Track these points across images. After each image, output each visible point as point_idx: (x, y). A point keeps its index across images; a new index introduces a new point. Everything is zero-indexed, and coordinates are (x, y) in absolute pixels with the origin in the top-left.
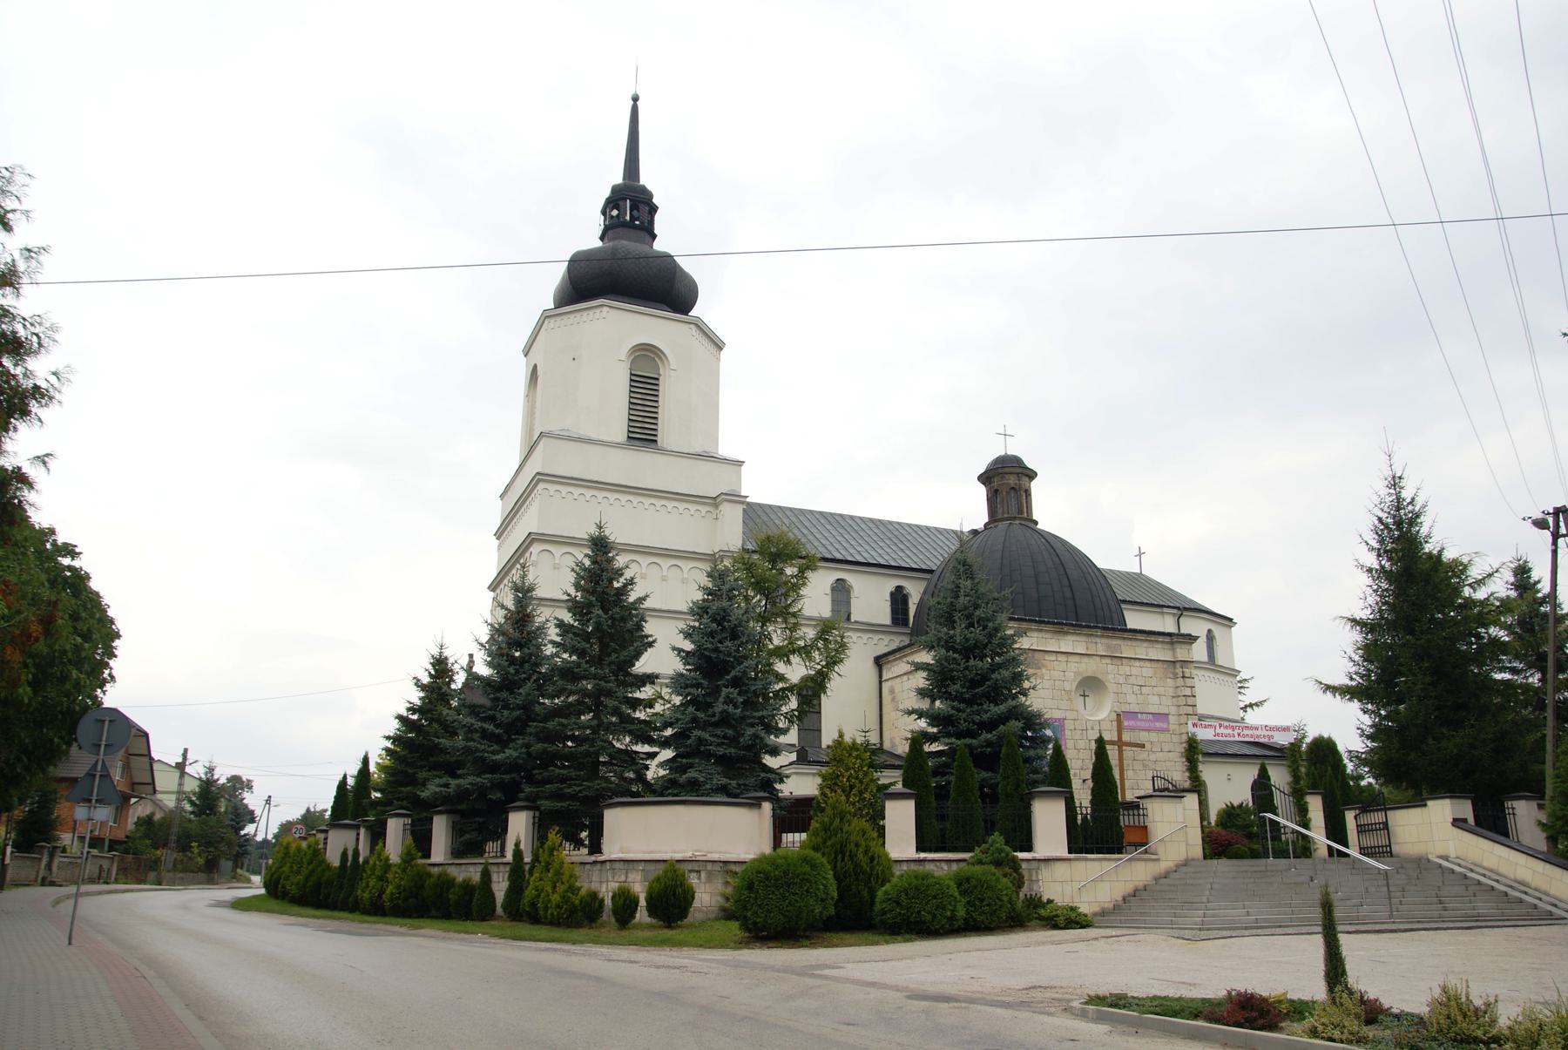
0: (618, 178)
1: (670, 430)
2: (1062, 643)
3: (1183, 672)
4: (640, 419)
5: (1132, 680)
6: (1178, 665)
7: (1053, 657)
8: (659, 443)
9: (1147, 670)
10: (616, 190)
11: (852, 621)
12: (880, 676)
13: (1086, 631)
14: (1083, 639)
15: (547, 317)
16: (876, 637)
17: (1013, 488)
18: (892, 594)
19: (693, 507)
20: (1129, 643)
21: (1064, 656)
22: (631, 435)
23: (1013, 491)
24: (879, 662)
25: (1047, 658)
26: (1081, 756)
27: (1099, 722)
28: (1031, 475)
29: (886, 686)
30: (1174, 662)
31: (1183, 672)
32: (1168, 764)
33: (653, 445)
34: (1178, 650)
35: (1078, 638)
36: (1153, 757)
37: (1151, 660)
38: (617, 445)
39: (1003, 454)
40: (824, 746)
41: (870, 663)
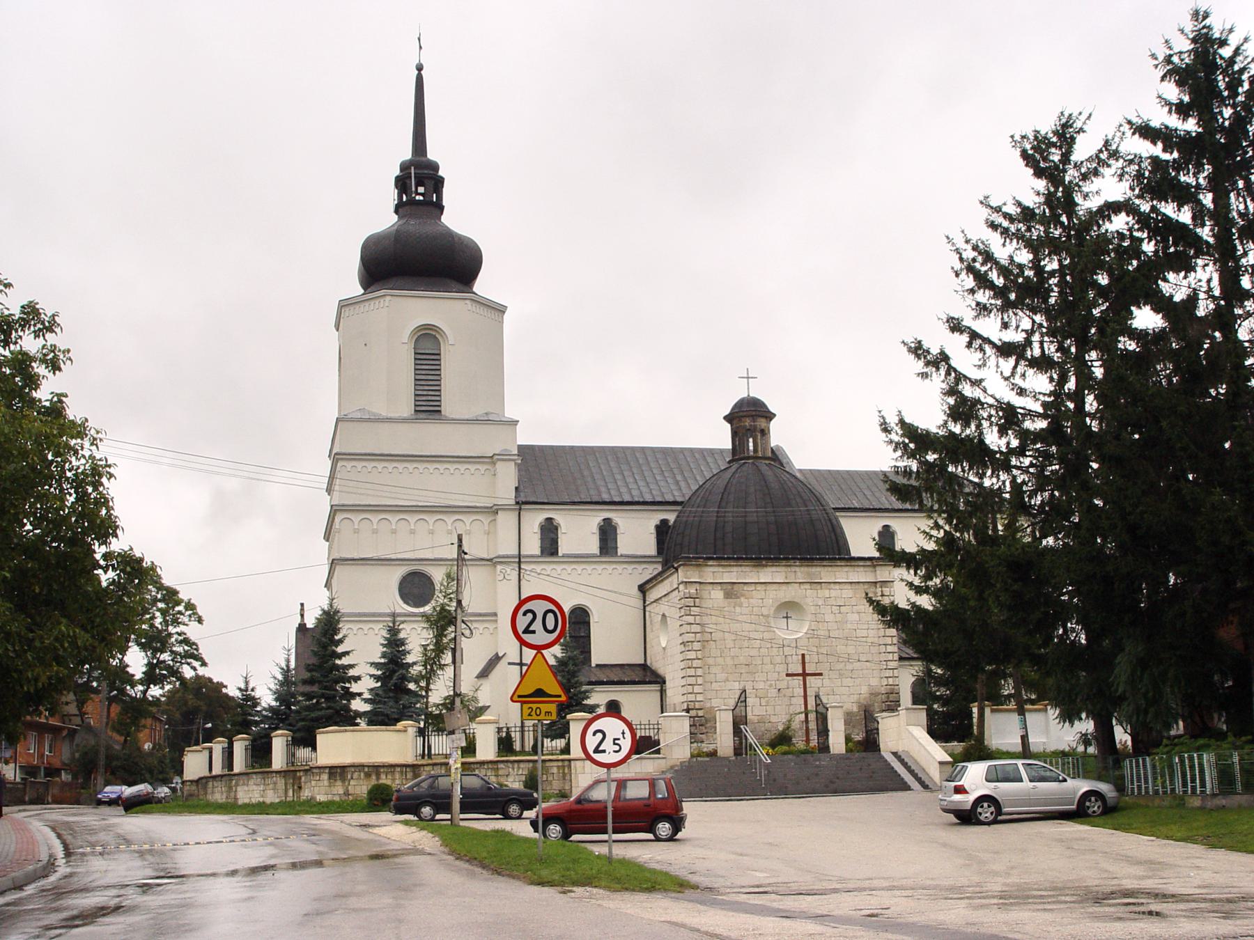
0: (407, 154)
1: (452, 401)
2: (761, 575)
3: (882, 591)
4: (425, 393)
5: (832, 602)
6: (878, 585)
7: (752, 587)
8: (443, 413)
9: (847, 592)
10: (405, 167)
11: (619, 554)
12: (644, 602)
13: (784, 563)
14: (783, 569)
15: (342, 306)
16: (640, 567)
17: (749, 430)
18: (657, 527)
19: (472, 467)
20: (830, 569)
21: (763, 585)
22: (418, 408)
23: (748, 432)
24: (643, 589)
25: (745, 588)
26: (777, 669)
27: (796, 640)
28: (770, 416)
29: (647, 609)
30: (876, 583)
31: (882, 591)
32: (865, 672)
33: (437, 416)
34: (878, 572)
35: (778, 569)
36: (849, 667)
37: (851, 583)
38: (404, 420)
39: (746, 395)
40: (593, 665)
41: (635, 591)
